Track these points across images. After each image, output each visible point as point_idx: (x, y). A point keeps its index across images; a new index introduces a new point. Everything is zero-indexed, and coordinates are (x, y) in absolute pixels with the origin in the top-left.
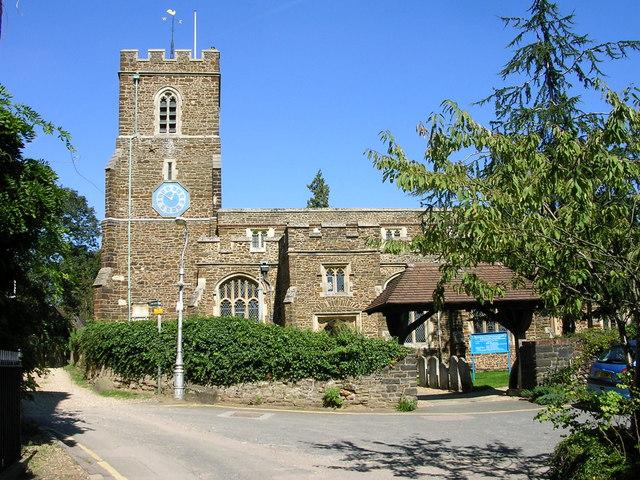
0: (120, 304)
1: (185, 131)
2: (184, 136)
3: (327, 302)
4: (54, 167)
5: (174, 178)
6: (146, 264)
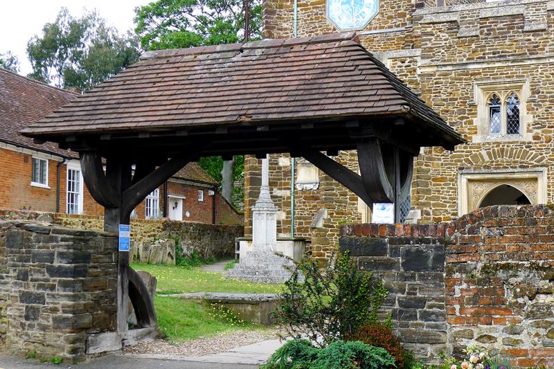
0: (281, 164)
3: (484, 153)
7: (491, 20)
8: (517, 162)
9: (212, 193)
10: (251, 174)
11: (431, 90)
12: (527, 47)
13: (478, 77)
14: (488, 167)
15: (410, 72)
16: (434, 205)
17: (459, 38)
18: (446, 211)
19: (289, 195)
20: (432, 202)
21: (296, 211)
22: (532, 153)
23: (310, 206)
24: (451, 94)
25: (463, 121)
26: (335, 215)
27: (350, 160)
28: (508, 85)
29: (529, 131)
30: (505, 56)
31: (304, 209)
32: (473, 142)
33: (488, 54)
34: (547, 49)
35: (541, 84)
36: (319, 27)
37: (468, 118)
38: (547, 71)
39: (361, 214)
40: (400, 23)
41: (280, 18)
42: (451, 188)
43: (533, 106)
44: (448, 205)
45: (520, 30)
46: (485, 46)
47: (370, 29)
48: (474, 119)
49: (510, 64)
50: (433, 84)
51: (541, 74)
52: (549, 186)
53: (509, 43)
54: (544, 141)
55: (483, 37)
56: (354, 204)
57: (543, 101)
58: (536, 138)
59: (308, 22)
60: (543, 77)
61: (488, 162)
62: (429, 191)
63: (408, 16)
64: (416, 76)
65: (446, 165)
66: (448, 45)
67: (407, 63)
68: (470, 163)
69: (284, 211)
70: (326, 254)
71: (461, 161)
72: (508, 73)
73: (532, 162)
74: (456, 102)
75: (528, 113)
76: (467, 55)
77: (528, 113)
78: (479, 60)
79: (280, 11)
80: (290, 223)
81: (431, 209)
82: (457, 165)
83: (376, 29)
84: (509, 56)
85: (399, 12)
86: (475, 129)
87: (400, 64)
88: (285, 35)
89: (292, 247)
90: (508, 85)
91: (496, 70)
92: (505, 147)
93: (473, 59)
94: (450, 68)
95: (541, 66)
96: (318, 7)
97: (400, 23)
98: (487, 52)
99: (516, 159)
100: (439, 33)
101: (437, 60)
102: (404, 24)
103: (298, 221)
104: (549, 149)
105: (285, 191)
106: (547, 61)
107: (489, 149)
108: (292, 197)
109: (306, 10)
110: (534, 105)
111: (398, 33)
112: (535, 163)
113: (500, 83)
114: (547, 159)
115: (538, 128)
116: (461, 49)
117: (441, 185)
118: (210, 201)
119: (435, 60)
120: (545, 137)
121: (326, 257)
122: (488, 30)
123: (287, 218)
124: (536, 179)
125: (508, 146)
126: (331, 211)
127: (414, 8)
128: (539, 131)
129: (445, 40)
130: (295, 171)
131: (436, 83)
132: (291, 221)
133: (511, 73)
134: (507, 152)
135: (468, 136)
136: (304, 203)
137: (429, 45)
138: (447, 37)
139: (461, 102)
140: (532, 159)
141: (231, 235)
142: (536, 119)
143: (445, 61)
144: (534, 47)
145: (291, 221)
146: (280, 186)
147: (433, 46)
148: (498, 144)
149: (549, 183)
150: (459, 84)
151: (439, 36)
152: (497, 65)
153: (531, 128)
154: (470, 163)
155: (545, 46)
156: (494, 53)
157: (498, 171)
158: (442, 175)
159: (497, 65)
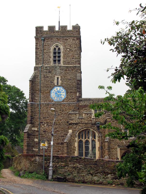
0: (35, 141)
2: (64, 65)
10: (27, 143)
16: (111, 155)
18: (115, 156)
27: (73, 141)
36: (48, 100)
41: (35, 96)
42: (116, 151)
47: (64, 102)
63: (75, 99)
65: (114, 144)
67: (89, 115)
68: (121, 144)
83: (65, 102)
87: (87, 115)
88: (36, 101)
96: (47, 94)
102: (74, 102)
109: (43, 94)
111: (73, 104)
131: (111, 123)
141: (128, 174)
154: (121, 144)
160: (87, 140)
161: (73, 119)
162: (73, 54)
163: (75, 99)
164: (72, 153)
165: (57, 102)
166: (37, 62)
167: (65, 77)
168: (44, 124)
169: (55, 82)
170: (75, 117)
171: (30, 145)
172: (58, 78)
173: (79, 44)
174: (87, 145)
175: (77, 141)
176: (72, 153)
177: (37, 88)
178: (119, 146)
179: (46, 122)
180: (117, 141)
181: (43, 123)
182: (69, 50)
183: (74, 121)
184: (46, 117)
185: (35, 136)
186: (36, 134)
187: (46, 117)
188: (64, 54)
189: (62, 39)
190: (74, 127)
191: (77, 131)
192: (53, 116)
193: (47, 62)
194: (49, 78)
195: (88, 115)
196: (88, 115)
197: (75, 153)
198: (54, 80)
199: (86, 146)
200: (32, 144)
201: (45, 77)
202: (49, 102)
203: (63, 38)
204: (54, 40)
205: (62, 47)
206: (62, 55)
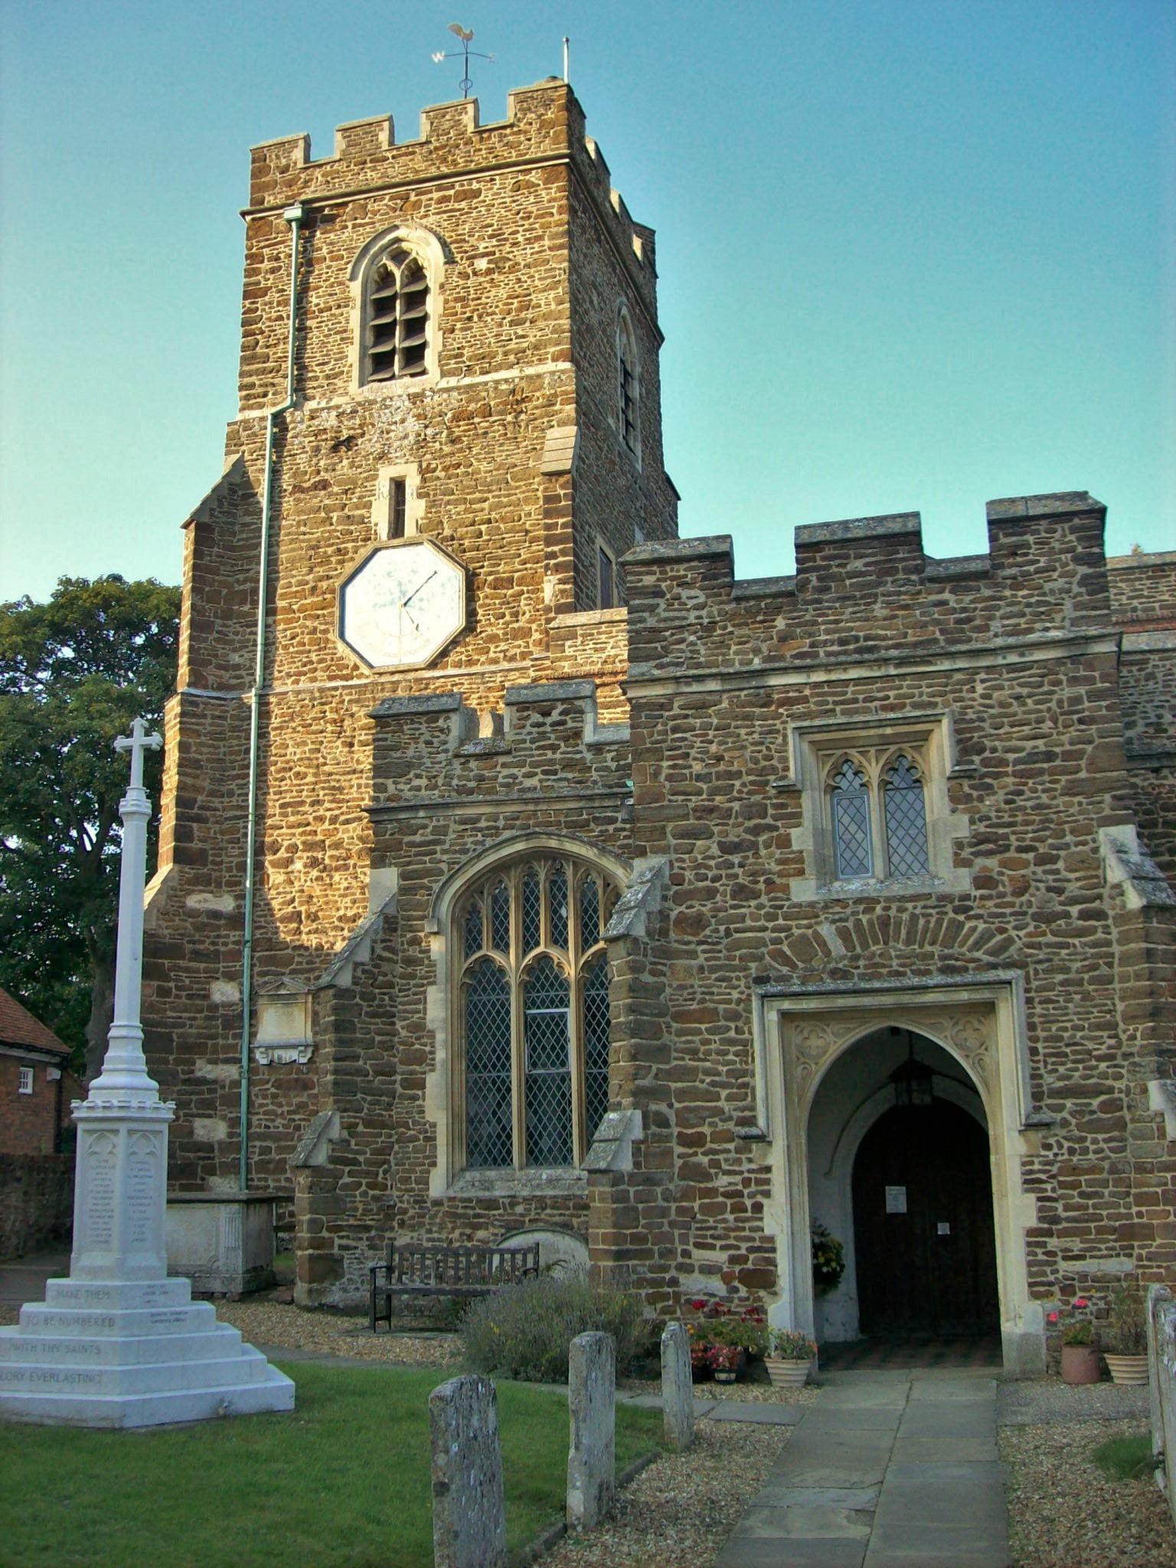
0: (217, 997)
1: (451, 364)
2: (453, 382)
3: (827, 930)
4: (92, 572)
5: (410, 530)
6: (309, 846)
7: (827, 552)
8: (931, 955)
9: (55, 1074)
11: (661, 750)
12: (937, 622)
13: (799, 708)
14: (845, 975)
15: (566, 739)
16: (681, 1095)
17: (738, 600)
18: (720, 1111)
19: (236, 1077)
20: (674, 1085)
21: (254, 1119)
22: (974, 929)
23: (289, 1104)
24: (719, 759)
25: (761, 839)
26: (361, 1128)
27: (403, 976)
28: (889, 731)
29: (960, 862)
30: (859, 651)
31: (274, 1113)
32: (795, 899)
33: (825, 643)
34: (996, 626)
35: (986, 725)
36: (321, 661)
37: (776, 828)
38: (1002, 688)
39: (434, 1125)
40: (518, 651)
41: (223, 639)
42: (732, 1042)
43: (966, 789)
44: (724, 1093)
45: (914, 577)
46: (815, 623)
48: (794, 832)
49: (893, 671)
50: (665, 733)
51: (983, 696)
52: (1032, 1027)
53: (885, 612)
54: (1009, 890)
55: (809, 596)
56: (414, 1098)
57: (997, 776)
58: (983, 881)
59: (291, 649)
60: (992, 707)
61: (843, 958)
62: (663, 1053)
63: (536, 636)
64: (580, 748)
65: (713, 969)
66: (706, 621)
67: (555, 716)
69: (224, 1118)
70: (337, 1242)
71: (760, 958)
72: (887, 698)
73: (978, 954)
74: (737, 783)
75: (954, 811)
76: (764, 647)
77: (954, 811)
78: (797, 662)
79: (224, 625)
80: (239, 1151)
81: (671, 1106)
82: (746, 969)
84: (887, 648)
85: (516, 625)
86: (799, 858)
87: (536, 717)
88: (234, 682)
89: (238, 1223)
90: (889, 731)
91: (851, 689)
92: (892, 913)
93: (782, 658)
94: (713, 685)
95: (983, 676)
97: (518, 651)
98: (823, 637)
99: (928, 948)
100: (677, 590)
101: (677, 665)
103: (258, 1143)
104: (1025, 914)
105: (226, 1067)
106: (1000, 661)
107: (841, 920)
108: (244, 1082)
110: (971, 787)
112: (987, 958)
113: (866, 726)
114: (1019, 943)
115: (989, 853)
116: (745, 631)
117: (699, 1032)
118: (51, 1097)
119: (668, 665)
120: (1011, 879)
121: (336, 1250)
122: (819, 579)
123: (230, 1135)
124: (989, 1009)
125: (901, 910)
126: (350, 1117)
127: (552, 615)
128: (992, 863)
129: (697, 607)
130: (253, 1014)
131: (675, 730)
132: (240, 1143)
133: (897, 697)
134: (898, 925)
135: (778, 881)
136: (275, 1096)
137: (651, 622)
138: (702, 599)
139: (752, 783)
140: (977, 946)
142: (981, 828)
143: (699, 666)
144: (958, 621)
145: (240, 1143)
146: (213, 1053)
147: (662, 625)
148: (868, 902)
149: (1030, 1016)
150: (743, 731)
151: (678, 598)
152: (853, 673)
153: (966, 853)
155: (991, 618)
156: (842, 642)
157: (877, 985)
158: (703, 1001)
159: (853, 673)
160: (544, 958)
161: (410, 766)
162: (519, 291)
163: (536, 636)
164: (399, 1090)
165: (393, 673)
166: (252, 386)
167: (458, 466)
168: (290, 861)
169: (380, 515)
170: (429, 743)
171: (161, 1035)
172: (399, 486)
173: (560, 207)
174: (543, 1004)
175: (441, 970)
176: (399, 1090)
177: (241, 577)
178: (772, 988)
179: (304, 843)
180: (749, 923)
181: (282, 854)
182: (489, 262)
183: (417, 782)
184: (302, 803)
185: (216, 956)
186: (225, 944)
187: (302, 803)
188: (446, 301)
189: (436, 195)
190: (417, 838)
191: (444, 879)
192: (359, 786)
193: (328, 377)
194: (336, 489)
195: (546, 714)
196: (549, 720)
197: (422, 1085)
198: (368, 506)
199: (534, 1017)
200: (183, 1025)
201: (303, 491)
202: (331, 678)
203: (440, 188)
204: (375, 213)
205: (429, 254)
206: (433, 305)
